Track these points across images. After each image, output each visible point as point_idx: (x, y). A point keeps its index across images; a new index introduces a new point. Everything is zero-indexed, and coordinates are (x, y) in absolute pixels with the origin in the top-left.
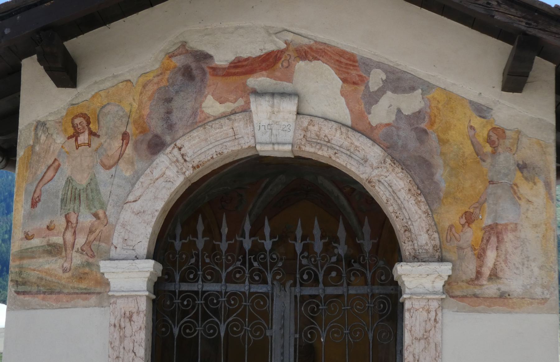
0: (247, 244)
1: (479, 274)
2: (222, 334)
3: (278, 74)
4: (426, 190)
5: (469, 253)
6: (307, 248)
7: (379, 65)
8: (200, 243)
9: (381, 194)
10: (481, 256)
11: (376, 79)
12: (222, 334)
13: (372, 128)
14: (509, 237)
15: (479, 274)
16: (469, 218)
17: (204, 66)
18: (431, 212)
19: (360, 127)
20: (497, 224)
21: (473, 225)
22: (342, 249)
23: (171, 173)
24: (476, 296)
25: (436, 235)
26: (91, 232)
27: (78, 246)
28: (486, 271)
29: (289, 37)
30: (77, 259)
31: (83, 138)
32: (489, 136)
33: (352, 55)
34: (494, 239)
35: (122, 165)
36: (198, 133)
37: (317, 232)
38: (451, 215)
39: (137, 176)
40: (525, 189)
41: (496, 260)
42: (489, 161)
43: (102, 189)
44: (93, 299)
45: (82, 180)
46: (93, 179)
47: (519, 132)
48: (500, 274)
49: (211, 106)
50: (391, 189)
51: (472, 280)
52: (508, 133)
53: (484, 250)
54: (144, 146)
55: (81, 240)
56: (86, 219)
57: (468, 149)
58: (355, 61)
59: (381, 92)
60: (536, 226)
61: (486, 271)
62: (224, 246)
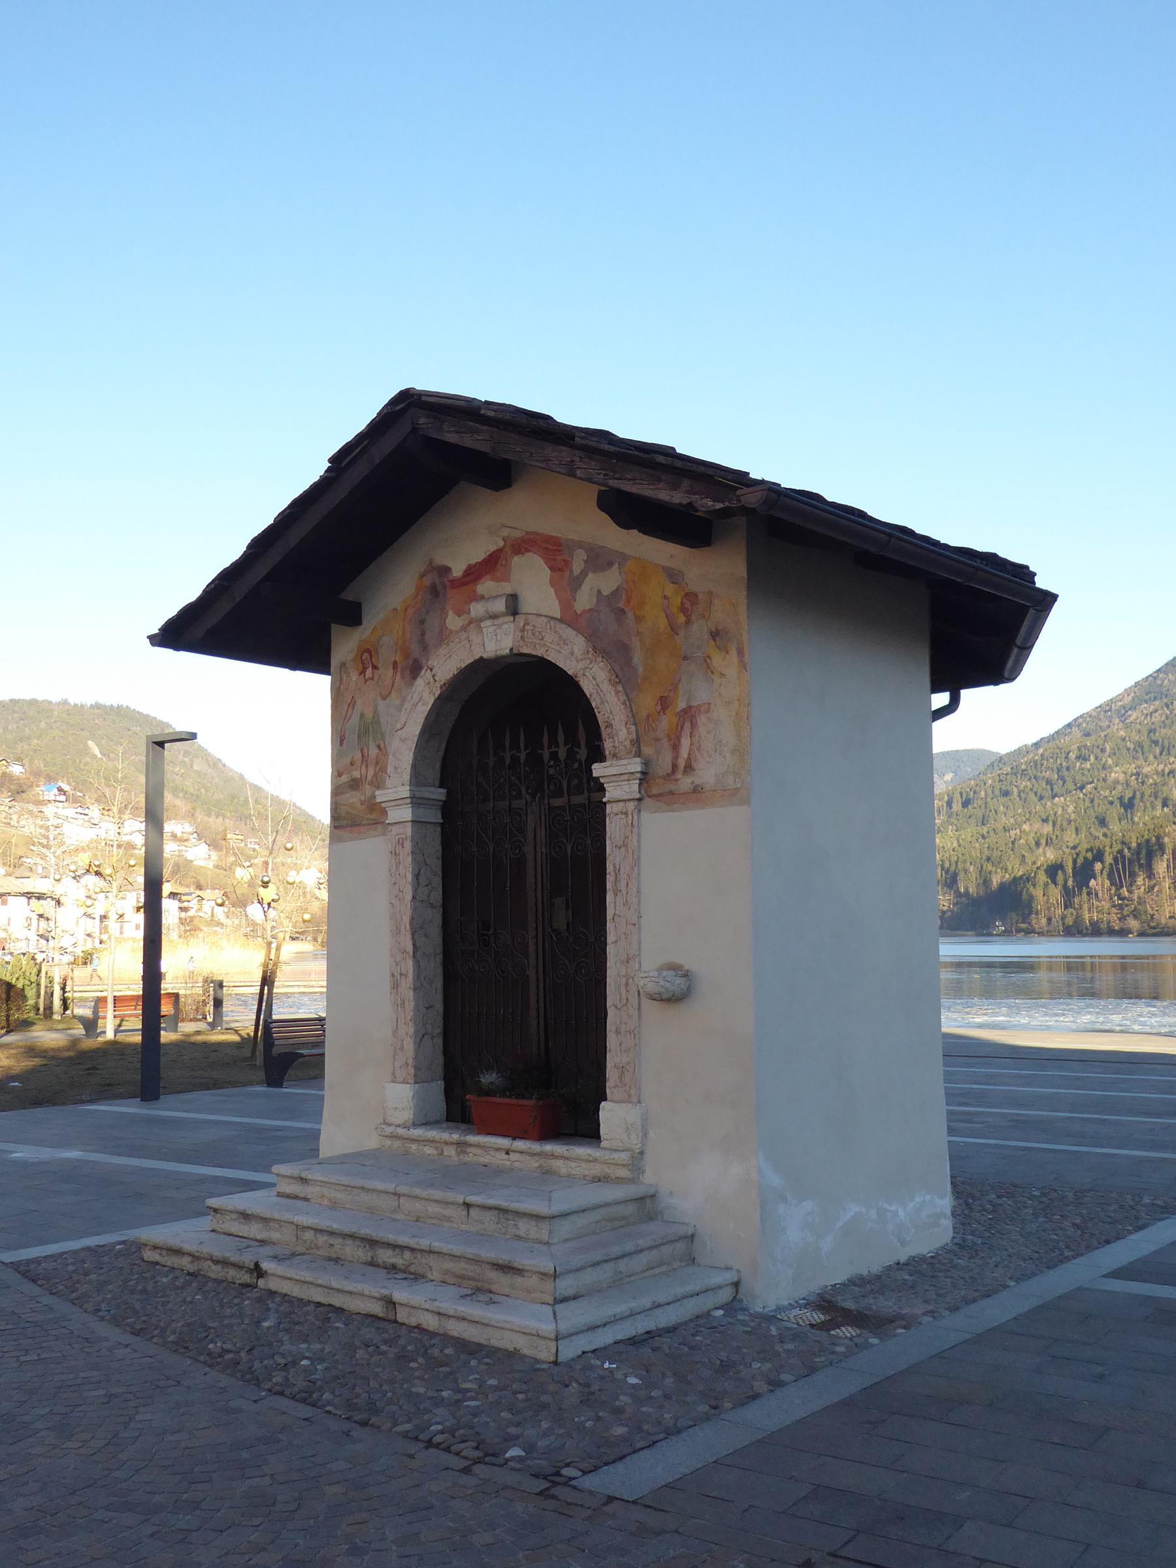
1: (675, 766)
2: (569, 852)
3: (498, 574)
4: (624, 677)
5: (665, 743)
6: (554, 756)
7: (580, 545)
9: (587, 686)
10: (676, 747)
11: (578, 562)
12: (569, 852)
13: (578, 616)
14: (702, 720)
15: (675, 766)
16: (664, 703)
17: (445, 580)
18: (629, 703)
19: (570, 618)
20: (690, 707)
21: (668, 711)
24: (671, 793)
25: (633, 728)
26: (377, 763)
27: (369, 778)
28: (682, 763)
29: (505, 532)
31: (369, 672)
32: (682, 604)
33: (558, 538)
34: (688, 725)
35: (393, 695)
37: (561, 738)
38: (647, 702)
39: (403, 700)
40: (717, 660)
41: (691, 750)
42: (682, 633)
43: (382, 720)
47: (710, 593)
48: (694, 765)
49: (453, 621)
50: (596, 681)
51: (668, 775)
52: (700, 597)
53: (679, 739)
54: (408, 672)
55: (371, 772)
56: (373, 752)
57: (663, 622)
58: (560, 545)
59: (584, 573)
60: (728, 703)
61: (682, 763)
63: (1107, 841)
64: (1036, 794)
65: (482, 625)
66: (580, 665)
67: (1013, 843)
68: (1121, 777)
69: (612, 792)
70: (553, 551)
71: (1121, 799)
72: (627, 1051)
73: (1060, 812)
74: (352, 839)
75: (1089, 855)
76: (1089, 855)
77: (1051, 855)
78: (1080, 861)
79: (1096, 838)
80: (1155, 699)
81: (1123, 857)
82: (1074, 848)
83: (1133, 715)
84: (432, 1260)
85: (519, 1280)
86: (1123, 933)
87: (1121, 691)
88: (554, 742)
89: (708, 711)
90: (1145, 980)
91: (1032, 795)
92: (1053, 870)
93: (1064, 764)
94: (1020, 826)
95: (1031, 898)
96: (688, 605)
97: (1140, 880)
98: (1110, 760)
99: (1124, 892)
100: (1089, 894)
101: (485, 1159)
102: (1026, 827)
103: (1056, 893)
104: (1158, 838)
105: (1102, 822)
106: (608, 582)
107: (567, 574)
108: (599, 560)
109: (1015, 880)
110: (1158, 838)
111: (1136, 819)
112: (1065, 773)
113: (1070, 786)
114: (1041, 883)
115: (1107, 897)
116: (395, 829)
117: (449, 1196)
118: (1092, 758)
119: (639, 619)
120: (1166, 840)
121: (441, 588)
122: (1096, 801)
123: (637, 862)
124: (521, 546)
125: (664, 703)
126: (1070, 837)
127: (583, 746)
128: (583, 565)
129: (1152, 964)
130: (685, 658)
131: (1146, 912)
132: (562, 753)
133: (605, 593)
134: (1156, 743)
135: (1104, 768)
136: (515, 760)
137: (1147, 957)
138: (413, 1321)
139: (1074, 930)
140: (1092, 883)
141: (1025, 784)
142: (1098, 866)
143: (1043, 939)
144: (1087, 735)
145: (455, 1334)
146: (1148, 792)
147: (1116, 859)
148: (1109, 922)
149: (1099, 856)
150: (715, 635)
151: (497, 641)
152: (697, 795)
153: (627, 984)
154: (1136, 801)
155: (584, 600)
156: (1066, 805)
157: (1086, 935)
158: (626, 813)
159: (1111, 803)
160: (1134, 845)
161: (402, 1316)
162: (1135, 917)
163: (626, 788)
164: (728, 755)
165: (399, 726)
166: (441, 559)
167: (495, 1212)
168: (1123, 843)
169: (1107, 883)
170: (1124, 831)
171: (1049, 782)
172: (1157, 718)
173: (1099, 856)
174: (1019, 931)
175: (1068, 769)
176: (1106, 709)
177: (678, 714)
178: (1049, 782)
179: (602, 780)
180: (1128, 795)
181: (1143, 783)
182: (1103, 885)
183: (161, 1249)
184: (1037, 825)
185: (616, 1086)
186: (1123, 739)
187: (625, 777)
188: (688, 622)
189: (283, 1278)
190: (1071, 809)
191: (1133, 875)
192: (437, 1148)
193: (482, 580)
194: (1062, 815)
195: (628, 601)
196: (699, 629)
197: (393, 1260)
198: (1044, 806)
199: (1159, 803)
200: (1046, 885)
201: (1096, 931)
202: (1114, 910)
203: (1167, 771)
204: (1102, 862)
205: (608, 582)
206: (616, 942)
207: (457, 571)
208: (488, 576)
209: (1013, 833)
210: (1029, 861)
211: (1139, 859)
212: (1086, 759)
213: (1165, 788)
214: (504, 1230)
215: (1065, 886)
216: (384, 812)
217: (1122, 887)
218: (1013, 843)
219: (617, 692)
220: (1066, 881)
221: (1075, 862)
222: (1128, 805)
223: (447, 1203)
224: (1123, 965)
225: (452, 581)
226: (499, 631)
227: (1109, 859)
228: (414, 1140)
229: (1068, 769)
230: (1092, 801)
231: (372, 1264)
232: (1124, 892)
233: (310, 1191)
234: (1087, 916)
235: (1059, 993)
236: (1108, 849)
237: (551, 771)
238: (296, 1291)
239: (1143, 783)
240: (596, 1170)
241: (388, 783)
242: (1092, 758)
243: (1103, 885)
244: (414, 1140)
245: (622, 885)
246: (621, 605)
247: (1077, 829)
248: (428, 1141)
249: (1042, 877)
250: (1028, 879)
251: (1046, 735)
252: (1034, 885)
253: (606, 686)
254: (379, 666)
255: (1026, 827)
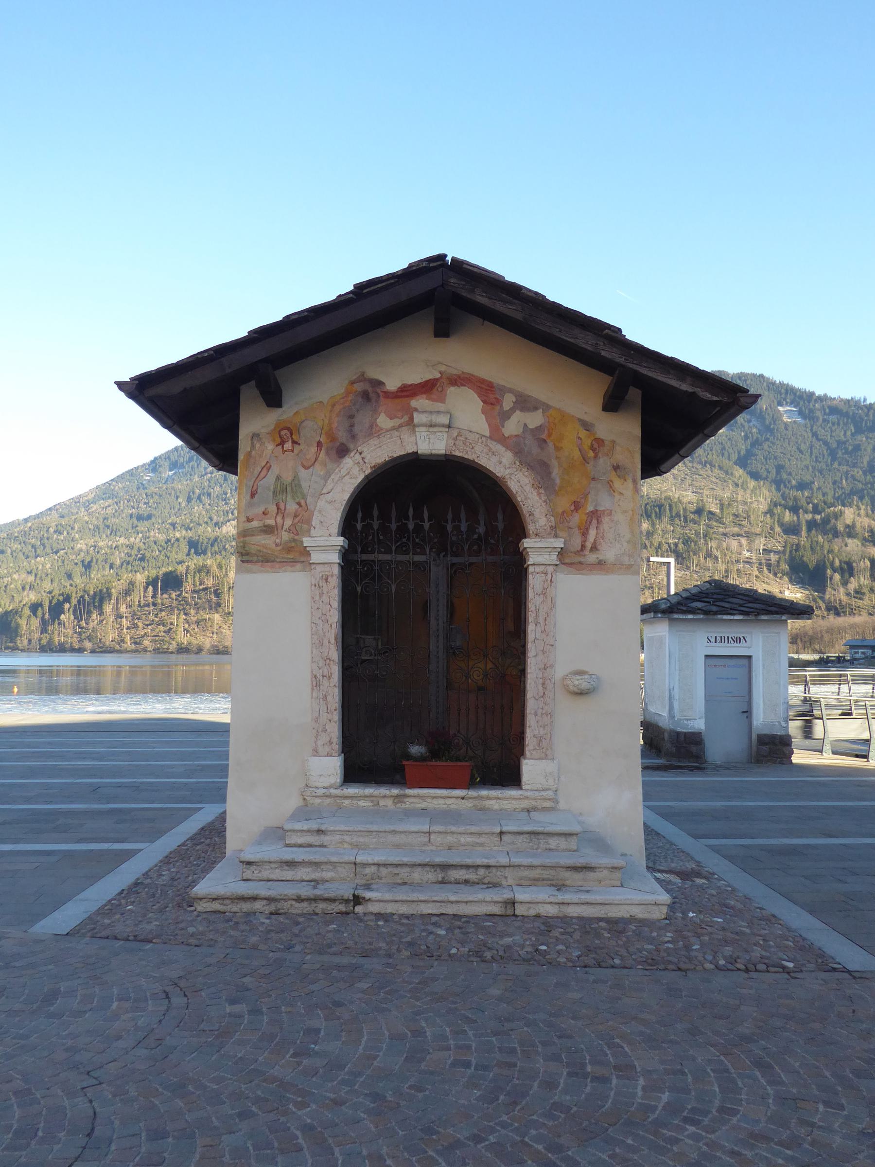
0: (411, 526)
1: (583, 547)
3: (434, 396)
6: (457, 528)
7: (511, 391)
8: (376, 524)
11: (508, 401)
14: (605, 520)
15: (583, 547)
16: (577, 506)
19: (497, 435)
21: (580, 511)
22: (481, 529)
23: (355, 471)
24: (580, 563)
26: (296, 516)
28: (589, 545)
30: (286, 536)
31: (288, 445)
32: (592, 444)
34: (594, 521)
36: (374, 442)
37: (463, 516)
38: (564, 503)
40: (617, 484)
41: (596, 537)
42: (592, 463)
43: (303, 484)
44: (299, 566)
45: (287, 477)
46: (296, 477)
48: (599, 547)
49: (383, 421)
50: (521, 485)
52: (606, 443)
53: (587, 529)
55: (288, 523)
56: (292, 507)
57: (577, 454)
58: (492, 387)
59: (512, 410)
60: (625, 512)
61: (589, 545)
62: (394, 526)
63: (74, 589)
64: (24, 554)
65: (417, 429)
66: (508, 471)
67: (6, 587)
68: (84, 547)
69: (533, 558)
70: (488, 392)
71: (83, 562)
72: (544, 726)
73: (40, 567)
74: (261, 572)
75: (61, 598)
76: (61, 598)
77: (33, 597)
78: (54, 602)
79: (65, 587)
80: (109, 498)
81: (84, 600)
82: (50, 593)
83: (94, 507)
84: (508, 872)
85: (591, 875)
86: (80, 650)
87: (87, 490)
88: (456, 518)
89: (610, 514)
90: (92, 680)
91: (21, 554)
92: (35, 607)
93: (46, 535)
94: (11, 575)
95: (18, 626)
96: (596, 446)
97: (94, 616)
98: (77, 536)
99: (83, 623)
100: (59, 624)
101: (424, 805)
102: (16, 576)
103: (36, 623)
104: (108, 589)
105: (69, 576)
106: (535, 420)
107: (498, 407)
108: (525, 403)
109: (7, 613)
110: (108, 589)
111: (92, 576)
112: (46, 541)
113: (48, 550)
114: (26, 616)
115: (71, 625)
116: (319, 568)
117: (486, 828)
118: (65, 533)
119: (558, 449)
120: (113, 591)
121: (370, 393)
122: (66, 562)
123: (553, 605)
124: (458, 380)
125: (577, 506)
126: (47, 585)
127: (482, 523)
128: (512, 405)
129: (97, 671)
130: (593, 479)
131: (97, 637)
132: (464, 527)
133: (531, 427)
134: (108, 527)
135: (73, 540)
136: (418, 529)
137: (95, 667)
138: (532, 912)
139: (47, 648)
140: (62, 617)
141: (16, 546)
142: (67, 606)
143: (24, 654)
144: (62, 517)
145: (575, 915)
146: (101, 559)
147: (79, 602)
148: (71, 643)
149: (68, 599)
150: (616, 468)
151: (430, 443)
152: (601, 566)
153: (543, 684)
154: (93, 564)
155: (512, 427)
156: (45, 563)
157: (56, 652)
158: (546, 574)
159: (76, 564)
160: (92, 593)
161: (520, 910)
162: (90, 641)
163: (547, 557)
164: (625, 544)
165: (325, 491)
166: (374, 373)
167: (527, 836)
168: (84, 591)
169: (72, 617)
170: (83, 583)
171: (33, 546)
172: (110, 511)
173: (68, 599)
174: (7, 648)
175: (48, 539)
176: (76, 501)
177: (587, 514)
178: (33, 546)
179: (528, 550)
180: (88, 559)
181: (98, 552)
182: (69, 618)
183: (223, 899)
184: (24, 576)
185: (535, 749)
186: (87, 523)
187: (549, 550)
188: (596, 457)
189: (381, 900)
190: (48, 566)
191: (89, 613)
192: (372, 801)
193: (418, 398)
194: (42, 570)
195: (550, 435)
196: (604, 463)
197: (467, 877)
198: (29, 563)
199: (107, 566)
200: (29, 617)
201: (62, 649)
202: (75, 635)
203: (114, 546)
204: (70, 603)
205: (535, 420)
206: (535, 656)
207: (392, 385)
208: (424, 396)
209: (5, 580)
210: (17, 600)
211: (94, 603)
212: (60, 533)
213: (112, 557)
214: (536, 847)
215: (43, 619)
216: (308, 554)
217: (82, 620)
218: (6, 587)
219: (539, 494)
220: (44, 615)
221: (50, 602)
222: (88, 566)
223: (480, 834)
224: (79, 672)
225: (385, 392)
226: (432, 436)
227: (74, 601)
228: (346, 797)
229: (48, 539)
230: (63, 562)
231: (443, 882)
232: (83, 623)
233: (325, 839)
234: (56, 639)
235: (30, 690)
236: (74, 595)
237: (454, 538)
238: (404, 909)
239: (98, 552)
240: (525, 804)
241: (313, 532)
242: (65, 533)
243: (69, 618)
244: (346, 797)
245: (541, 620)
246: (544, 436)
247: (52, 580)
248: (367, 796)
249: (27, 611)
250: (16, 613)
251: (33, 514)
252: (21, 617)
253: (528, 488)
254: (300, 442)
255: (16, 576)
